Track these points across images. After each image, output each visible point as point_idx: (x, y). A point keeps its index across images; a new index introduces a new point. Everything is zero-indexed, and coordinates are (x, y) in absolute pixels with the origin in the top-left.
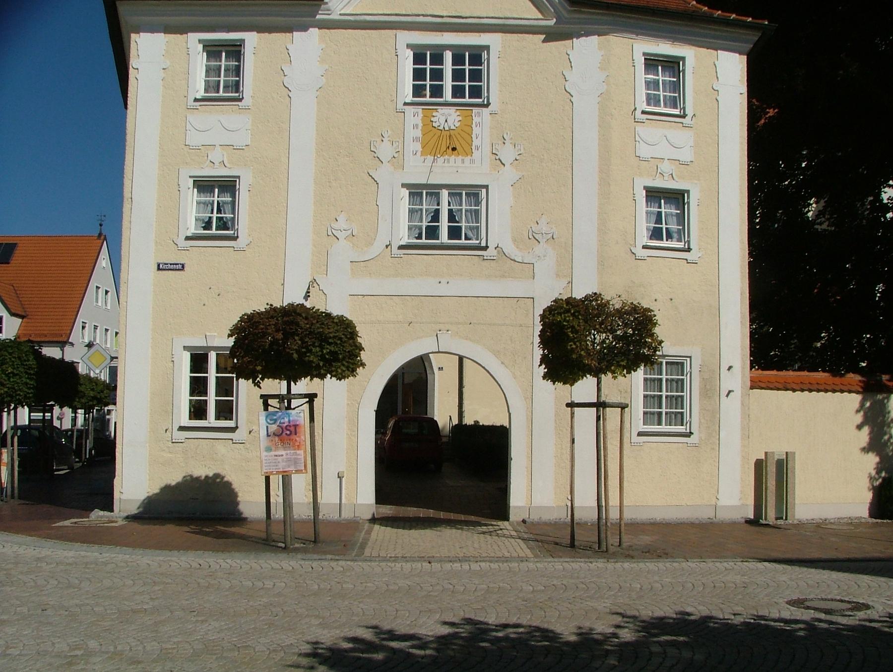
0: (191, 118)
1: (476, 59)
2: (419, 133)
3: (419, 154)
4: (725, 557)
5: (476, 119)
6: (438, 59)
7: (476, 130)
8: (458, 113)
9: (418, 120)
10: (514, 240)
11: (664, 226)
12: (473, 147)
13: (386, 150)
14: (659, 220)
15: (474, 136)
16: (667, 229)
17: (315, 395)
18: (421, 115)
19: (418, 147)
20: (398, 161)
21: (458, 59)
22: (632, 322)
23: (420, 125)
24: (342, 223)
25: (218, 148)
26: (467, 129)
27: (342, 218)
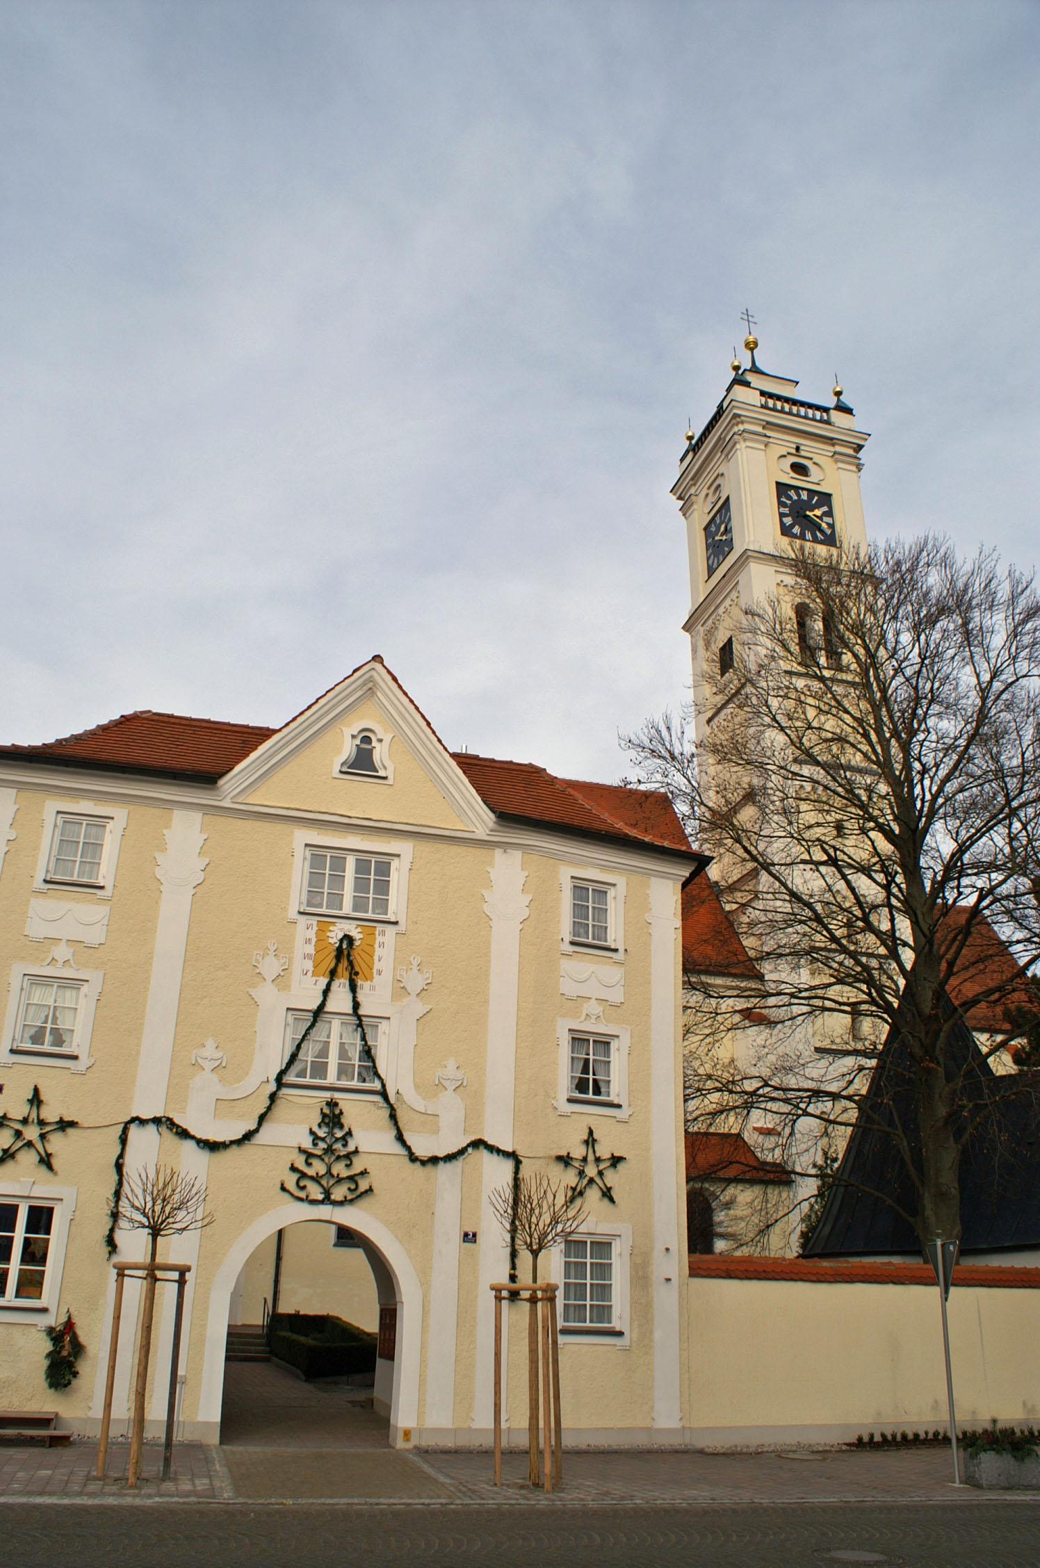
0: (567, 965)
1: (384, 869)
2: (311, 949)
3: (310, 974)
4: (687, 1512)
5: (379, 939)
6: (339, 864)
7: (378, 952)
8: (359, 930)
9: (312, 934)
10: (417, 1086)
11: (591, 1076)
12: (375, 971)
13: (271, 967)
14: (585, 1070)
15: (376, 958)
16: (594, 1080)
17: (189, 1269)
18: (315, 928)
19: (309, 965)
20: (281, 980)
21: (362, 867)
22: (316, 1179)
23: (314, 940)
24: (210, 1050)
25: (593, 1001)
26: (367, 949)
27: (210, 1044)
